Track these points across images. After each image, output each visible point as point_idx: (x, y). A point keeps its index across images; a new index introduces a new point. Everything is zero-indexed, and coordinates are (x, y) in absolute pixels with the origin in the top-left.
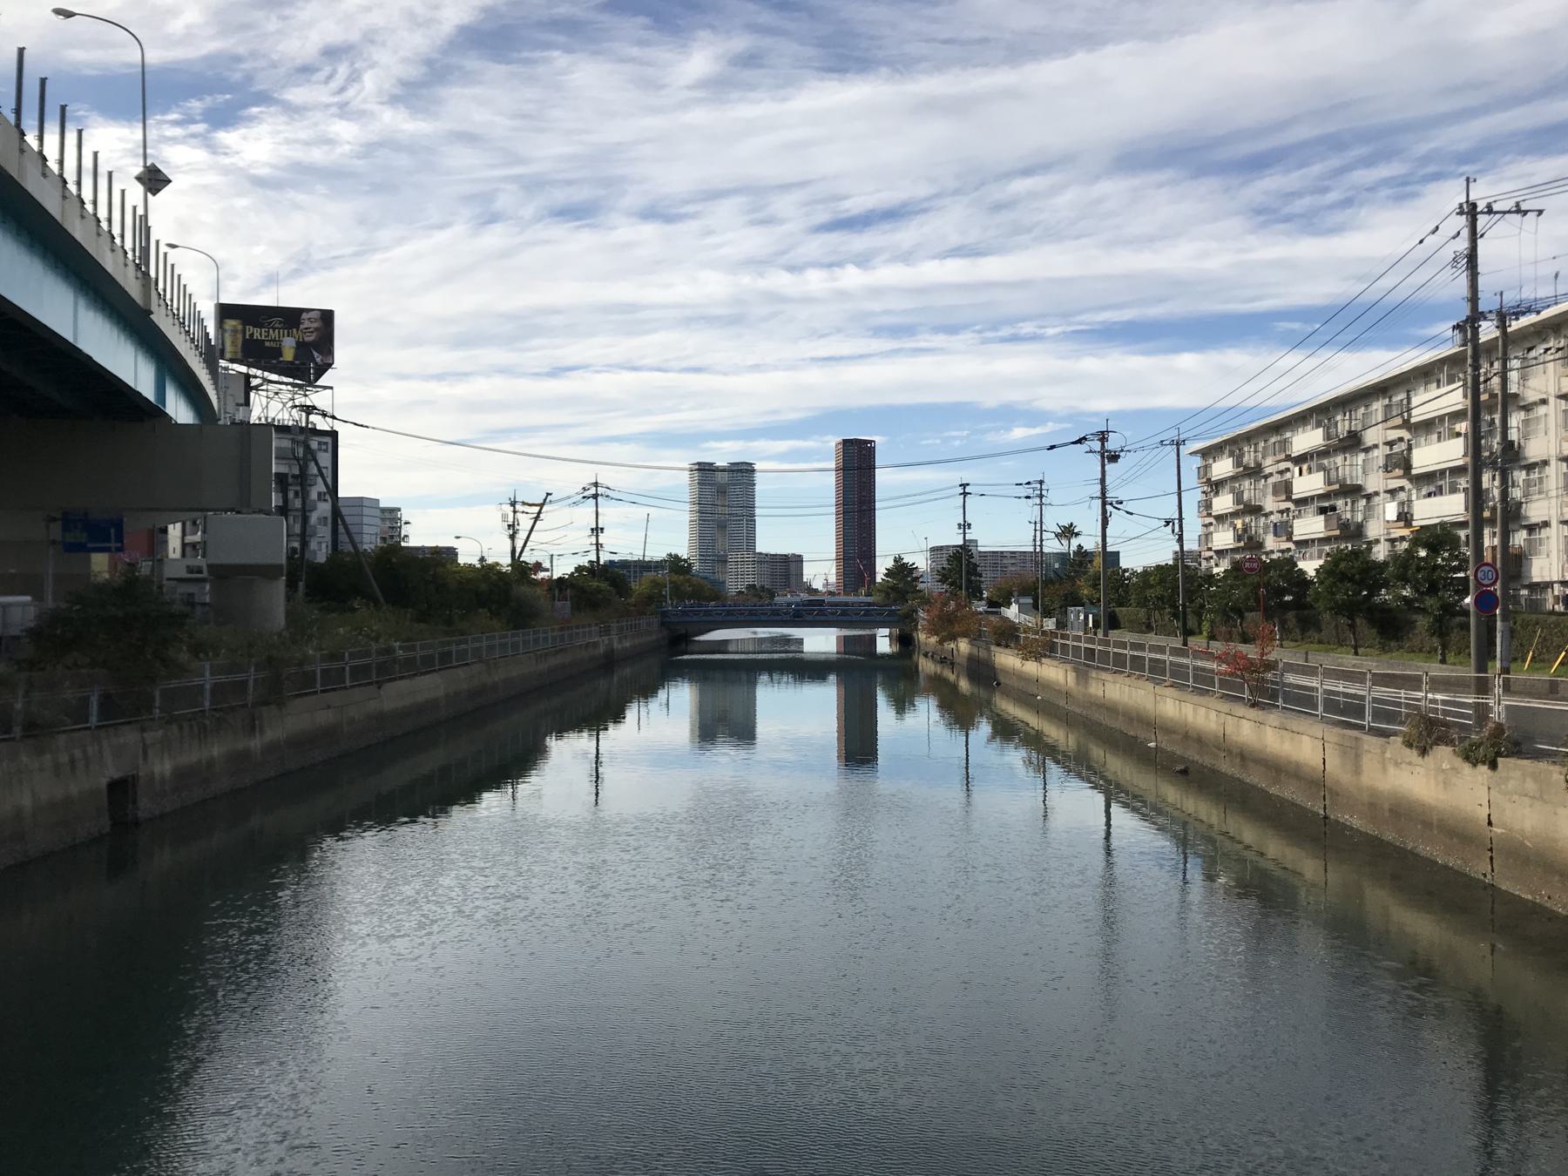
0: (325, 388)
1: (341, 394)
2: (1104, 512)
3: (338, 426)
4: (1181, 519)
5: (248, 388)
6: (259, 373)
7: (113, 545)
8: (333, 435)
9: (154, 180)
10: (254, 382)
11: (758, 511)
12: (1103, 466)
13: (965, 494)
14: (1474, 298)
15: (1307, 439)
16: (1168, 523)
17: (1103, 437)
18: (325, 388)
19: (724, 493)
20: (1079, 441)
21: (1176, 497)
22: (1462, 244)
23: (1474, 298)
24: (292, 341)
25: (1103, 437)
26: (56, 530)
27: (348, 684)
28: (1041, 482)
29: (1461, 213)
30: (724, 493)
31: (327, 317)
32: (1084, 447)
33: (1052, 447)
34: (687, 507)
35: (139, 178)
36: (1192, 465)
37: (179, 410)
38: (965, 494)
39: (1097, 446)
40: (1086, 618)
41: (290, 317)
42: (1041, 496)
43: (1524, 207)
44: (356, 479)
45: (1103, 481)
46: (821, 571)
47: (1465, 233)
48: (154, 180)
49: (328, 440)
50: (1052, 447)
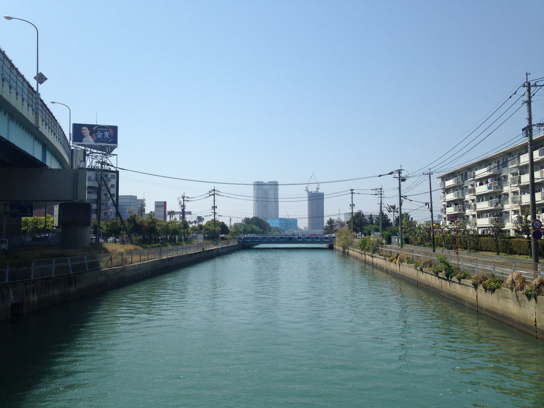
0: (114, 155)
1: (121, 158)
2: (400, 200)
3: (118, 170)
4: (431, 203)
5: (85, 155)
6: (89, 149)
7: (29, 214)
8: (117, 172)
9: (41, 78)
10: (88, 153)
11: (279, 200)
12: (400, 183)
13: (352, 193)
14: (530, 119)
15: (482, 172)
16: (426, 204)
17: (399, 172)
18: (114, 155)
19: (266, 193)
20: (390, 174)
21: (429, 194)
22: (526, 98)
23: (530, 119)
24: (106, 137)
25: (399, 172)
26: (8, 209)
27: (87, 270)
28: (381, 189)
29: (524, 86)
30: (266, 193)
31: (115, 129)
32: (393, 175)
33: (380, 176)
34: (252, 199)
35: (35, 78)
36: (437, 183)
37: (52, 164)
38: (352, 193)
39: (397, 175)
40: (398, 240)
41: (103, 128)
42: (381, 194)
43: (537, 84)
44: (126, 188)
45: (400, 188)
46: (303, 224)
47: (527, 94)
48: (41, 78)
49: (115, 174)
50: (380, 176)
